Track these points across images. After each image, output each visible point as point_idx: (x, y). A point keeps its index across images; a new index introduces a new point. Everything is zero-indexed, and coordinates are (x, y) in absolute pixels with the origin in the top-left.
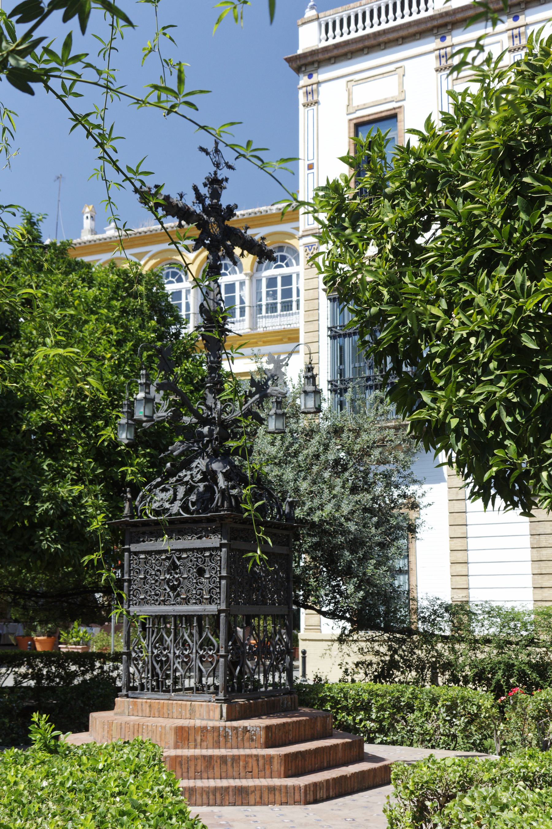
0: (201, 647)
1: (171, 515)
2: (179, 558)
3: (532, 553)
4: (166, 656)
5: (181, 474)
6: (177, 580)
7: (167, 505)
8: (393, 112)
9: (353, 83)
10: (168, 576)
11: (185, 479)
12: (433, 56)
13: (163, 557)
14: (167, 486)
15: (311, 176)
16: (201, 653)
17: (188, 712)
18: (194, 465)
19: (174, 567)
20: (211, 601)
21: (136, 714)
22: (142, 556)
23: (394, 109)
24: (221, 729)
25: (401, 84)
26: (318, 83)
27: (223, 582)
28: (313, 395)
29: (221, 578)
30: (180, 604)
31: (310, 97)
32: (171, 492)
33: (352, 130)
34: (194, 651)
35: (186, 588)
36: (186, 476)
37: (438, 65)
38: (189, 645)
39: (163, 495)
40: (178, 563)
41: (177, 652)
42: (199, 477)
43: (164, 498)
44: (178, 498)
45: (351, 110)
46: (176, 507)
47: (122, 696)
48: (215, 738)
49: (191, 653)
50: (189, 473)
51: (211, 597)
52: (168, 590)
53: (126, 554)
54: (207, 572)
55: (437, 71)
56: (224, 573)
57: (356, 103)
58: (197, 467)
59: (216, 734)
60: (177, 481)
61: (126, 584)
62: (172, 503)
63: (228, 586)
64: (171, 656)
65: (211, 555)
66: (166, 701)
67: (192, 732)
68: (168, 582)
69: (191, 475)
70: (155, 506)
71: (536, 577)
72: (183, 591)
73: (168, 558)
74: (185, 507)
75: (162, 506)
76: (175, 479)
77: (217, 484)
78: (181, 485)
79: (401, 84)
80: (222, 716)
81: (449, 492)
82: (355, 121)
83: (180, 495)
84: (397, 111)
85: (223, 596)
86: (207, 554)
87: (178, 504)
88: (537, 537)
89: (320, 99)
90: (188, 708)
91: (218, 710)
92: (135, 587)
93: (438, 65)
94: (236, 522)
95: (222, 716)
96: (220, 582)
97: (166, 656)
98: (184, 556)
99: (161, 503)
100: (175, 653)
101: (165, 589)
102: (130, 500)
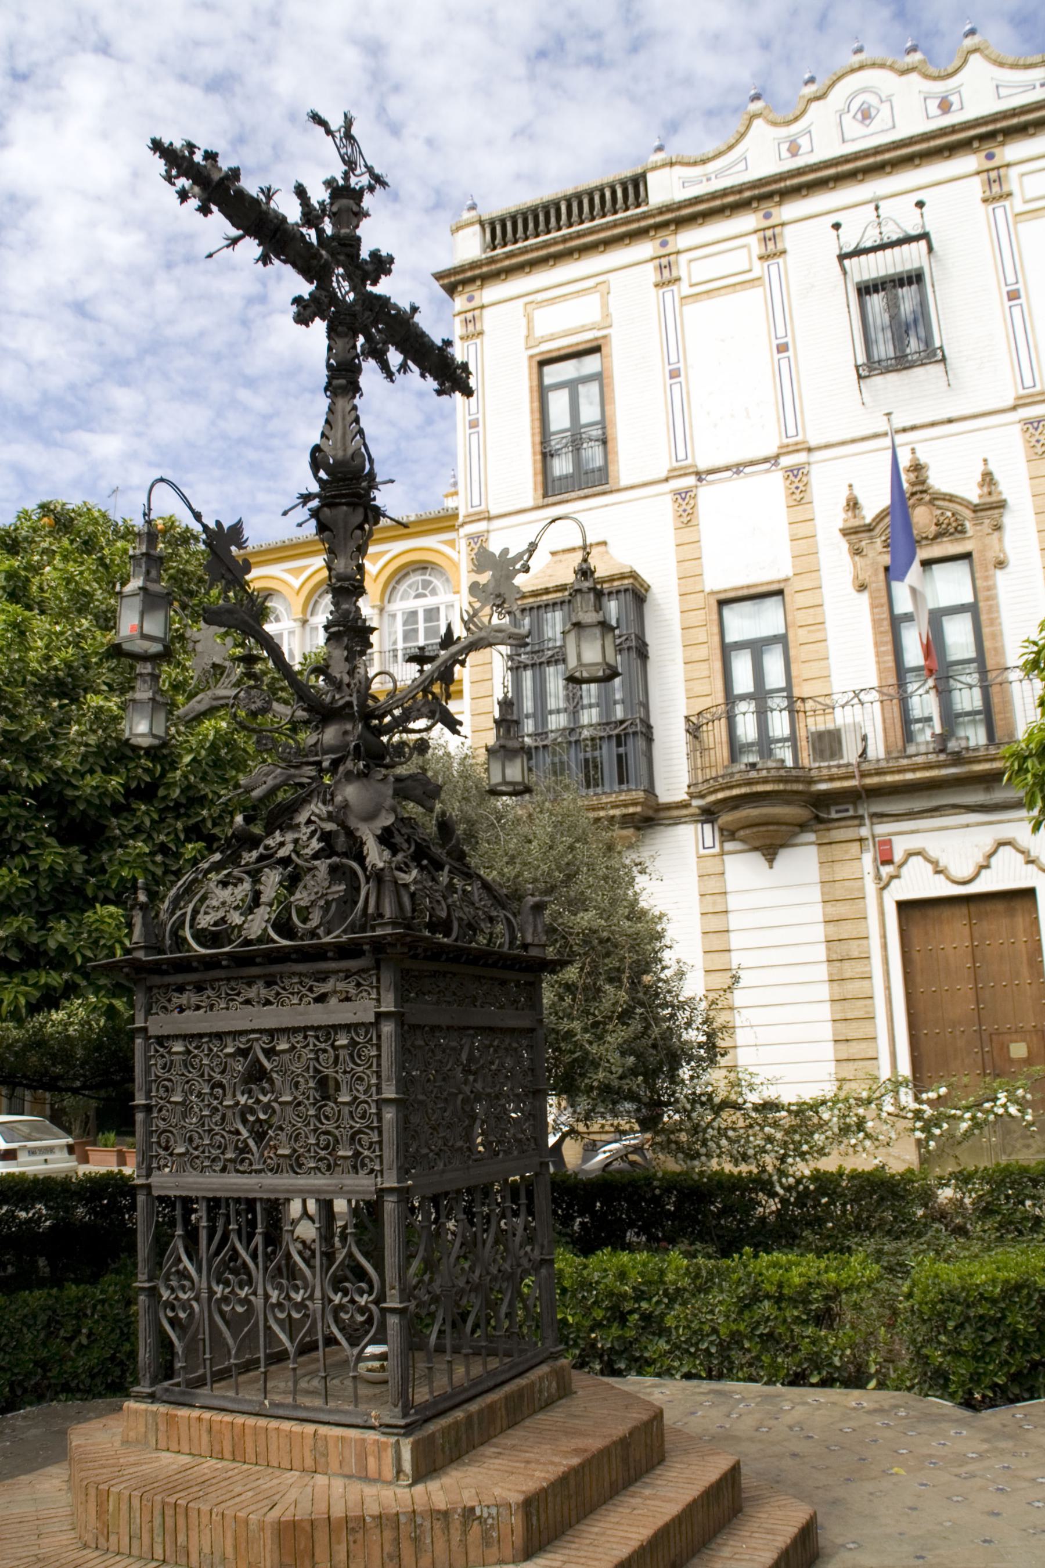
0: (337, 1284)
1: (248, 942)
2: (269, 1053)
3: (831, 989)
4: (246, 1301)
5: (270, 842)
6: (267, 1107)
7: (236, 918)
8: (594, 344)
9: (534, 306)
10: (243, 1100)
11: (282, 853)
12: (651, 266)
13: (230, 1050)
14: (236, 872)
15: (474, 437)
16: (337, 1299)
17: (307, 1454)
18: (302, 818)
19: (257, 1075)
20: (357, 1163)
21: (174, 1446)
22: (178, 1047)
23: (596, 339)
24: (403, 1519)
25: (605, 305)
26: (482, 307)
27: (389, 1115)
28: (597, 631)
29: (381, 1103)
30: (276, 1170)
31: (471, 327)
32: (247, 886)
33: (535, 370)
34: (318, 1294)
35: (289, 1129)
36: (282, 844)
37: (659, 278)
38: (304, 1278)
39: (225, 894)
40: (267, 1065)
41: (274, 1295)
42: (315, 845)
43: (230, 900)
44: (264, 899)
45: (531, 343)
46: (257, 924)
47: (139, 1397)
48: (388, 1548)
49: (311, 1297)
50: (290, 836)
51: (357, 1154)
52: (245, 1133)
53: (138, 1041)
54: (344, 1088)
55: (656, 285)
56: (390, 1092)
57: (539, 331)
58: (309, 822)
59: (388, 1534)
60: (261, 858)
61: (140, 1117)
62: (250, 910)
63: (404, 1126)
64: (258, 1302)
65: (353, 1043)
66: (251, 1421)
67: (321, 1536)
68: (244, 1112)
69: (296, 841)
70: (205, 921)
71: (838, 1025)
72: (283, 1136)
73: (243, 1053)
74: (283, 926)
75: (223, 920)
76: (255, 854)
77: (361, 859)
78: (271, 867)
79: (605, 305)
80: (399, 1471)
81: (701, 902)
82: (538, 358)
83: (268, 893)
84: (600, 342)
85: (389, 1153)
86: (342, 1041)
87: (262, 913)
88: (838, 964)
89: (486, 328)
90: (309, 1442)
91: (389, 1456)
92: (162, 1125)
93: (659, 278)
94: (415, 957)
95: (399, 1471)
96: (379, 1116)
97: (246, 1301)
98: (283, 1046)
99: (221, 914)
100: (267, 1297)
101: (238, 1133)
102: (143, 907)
